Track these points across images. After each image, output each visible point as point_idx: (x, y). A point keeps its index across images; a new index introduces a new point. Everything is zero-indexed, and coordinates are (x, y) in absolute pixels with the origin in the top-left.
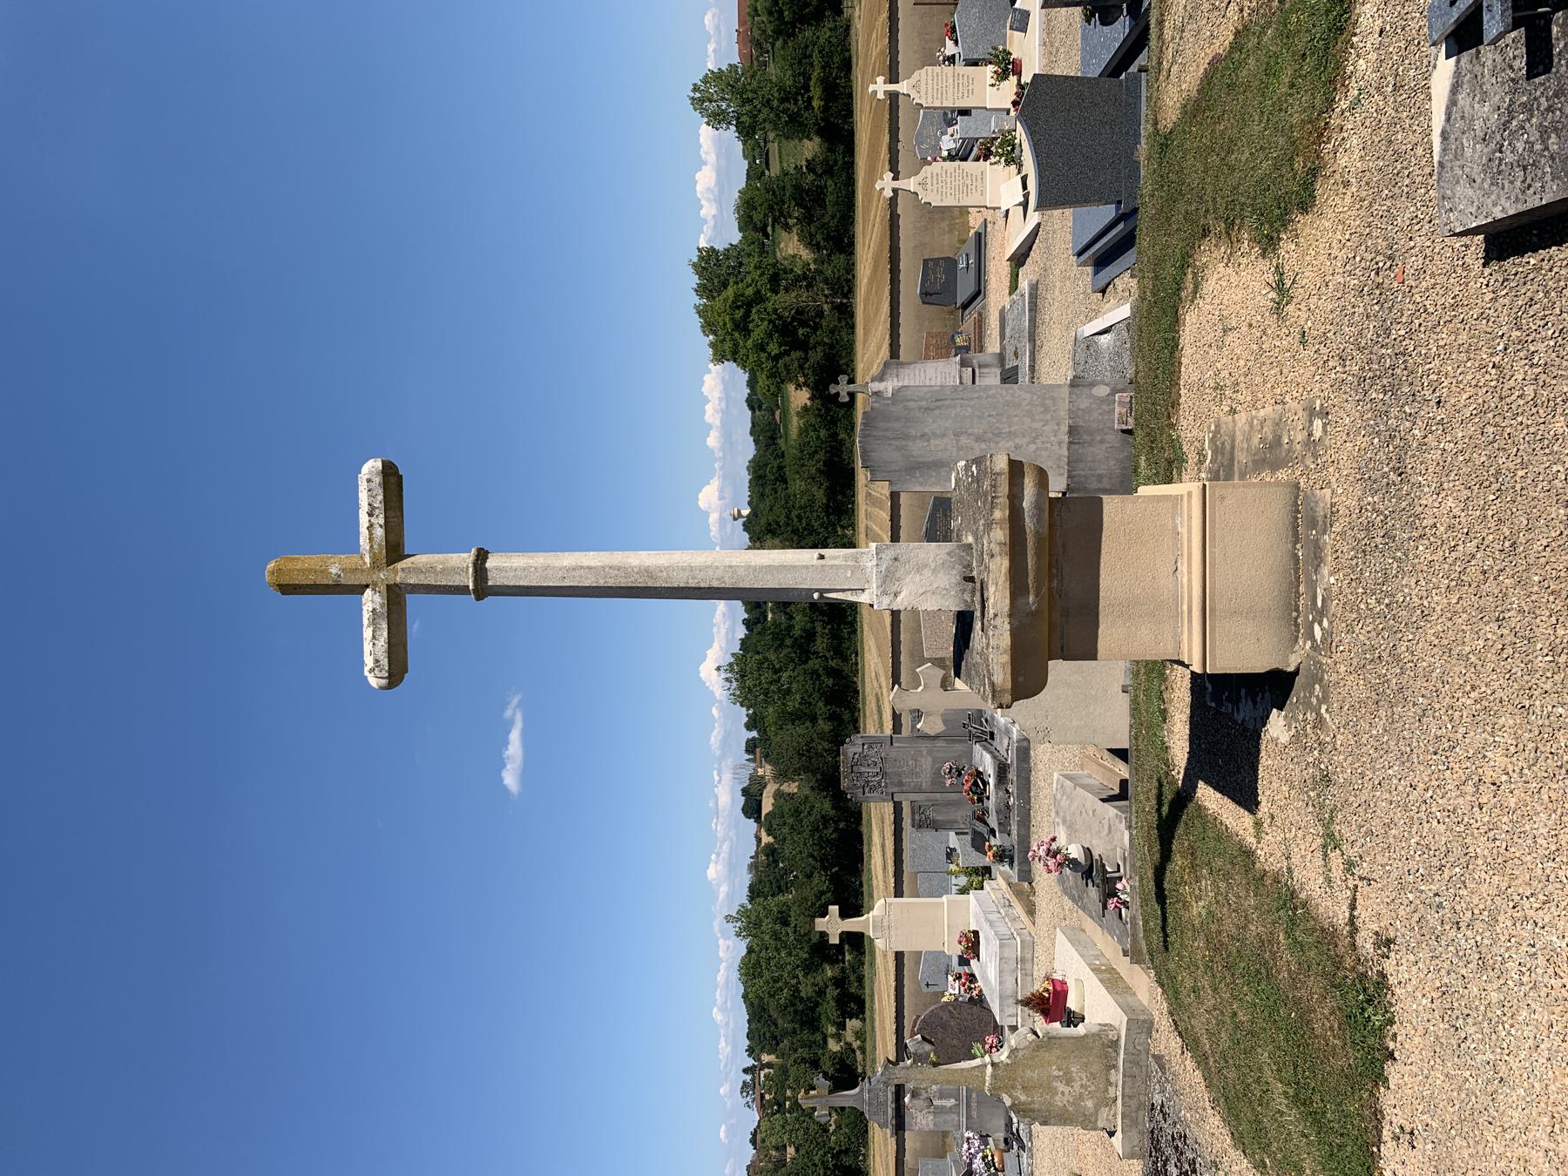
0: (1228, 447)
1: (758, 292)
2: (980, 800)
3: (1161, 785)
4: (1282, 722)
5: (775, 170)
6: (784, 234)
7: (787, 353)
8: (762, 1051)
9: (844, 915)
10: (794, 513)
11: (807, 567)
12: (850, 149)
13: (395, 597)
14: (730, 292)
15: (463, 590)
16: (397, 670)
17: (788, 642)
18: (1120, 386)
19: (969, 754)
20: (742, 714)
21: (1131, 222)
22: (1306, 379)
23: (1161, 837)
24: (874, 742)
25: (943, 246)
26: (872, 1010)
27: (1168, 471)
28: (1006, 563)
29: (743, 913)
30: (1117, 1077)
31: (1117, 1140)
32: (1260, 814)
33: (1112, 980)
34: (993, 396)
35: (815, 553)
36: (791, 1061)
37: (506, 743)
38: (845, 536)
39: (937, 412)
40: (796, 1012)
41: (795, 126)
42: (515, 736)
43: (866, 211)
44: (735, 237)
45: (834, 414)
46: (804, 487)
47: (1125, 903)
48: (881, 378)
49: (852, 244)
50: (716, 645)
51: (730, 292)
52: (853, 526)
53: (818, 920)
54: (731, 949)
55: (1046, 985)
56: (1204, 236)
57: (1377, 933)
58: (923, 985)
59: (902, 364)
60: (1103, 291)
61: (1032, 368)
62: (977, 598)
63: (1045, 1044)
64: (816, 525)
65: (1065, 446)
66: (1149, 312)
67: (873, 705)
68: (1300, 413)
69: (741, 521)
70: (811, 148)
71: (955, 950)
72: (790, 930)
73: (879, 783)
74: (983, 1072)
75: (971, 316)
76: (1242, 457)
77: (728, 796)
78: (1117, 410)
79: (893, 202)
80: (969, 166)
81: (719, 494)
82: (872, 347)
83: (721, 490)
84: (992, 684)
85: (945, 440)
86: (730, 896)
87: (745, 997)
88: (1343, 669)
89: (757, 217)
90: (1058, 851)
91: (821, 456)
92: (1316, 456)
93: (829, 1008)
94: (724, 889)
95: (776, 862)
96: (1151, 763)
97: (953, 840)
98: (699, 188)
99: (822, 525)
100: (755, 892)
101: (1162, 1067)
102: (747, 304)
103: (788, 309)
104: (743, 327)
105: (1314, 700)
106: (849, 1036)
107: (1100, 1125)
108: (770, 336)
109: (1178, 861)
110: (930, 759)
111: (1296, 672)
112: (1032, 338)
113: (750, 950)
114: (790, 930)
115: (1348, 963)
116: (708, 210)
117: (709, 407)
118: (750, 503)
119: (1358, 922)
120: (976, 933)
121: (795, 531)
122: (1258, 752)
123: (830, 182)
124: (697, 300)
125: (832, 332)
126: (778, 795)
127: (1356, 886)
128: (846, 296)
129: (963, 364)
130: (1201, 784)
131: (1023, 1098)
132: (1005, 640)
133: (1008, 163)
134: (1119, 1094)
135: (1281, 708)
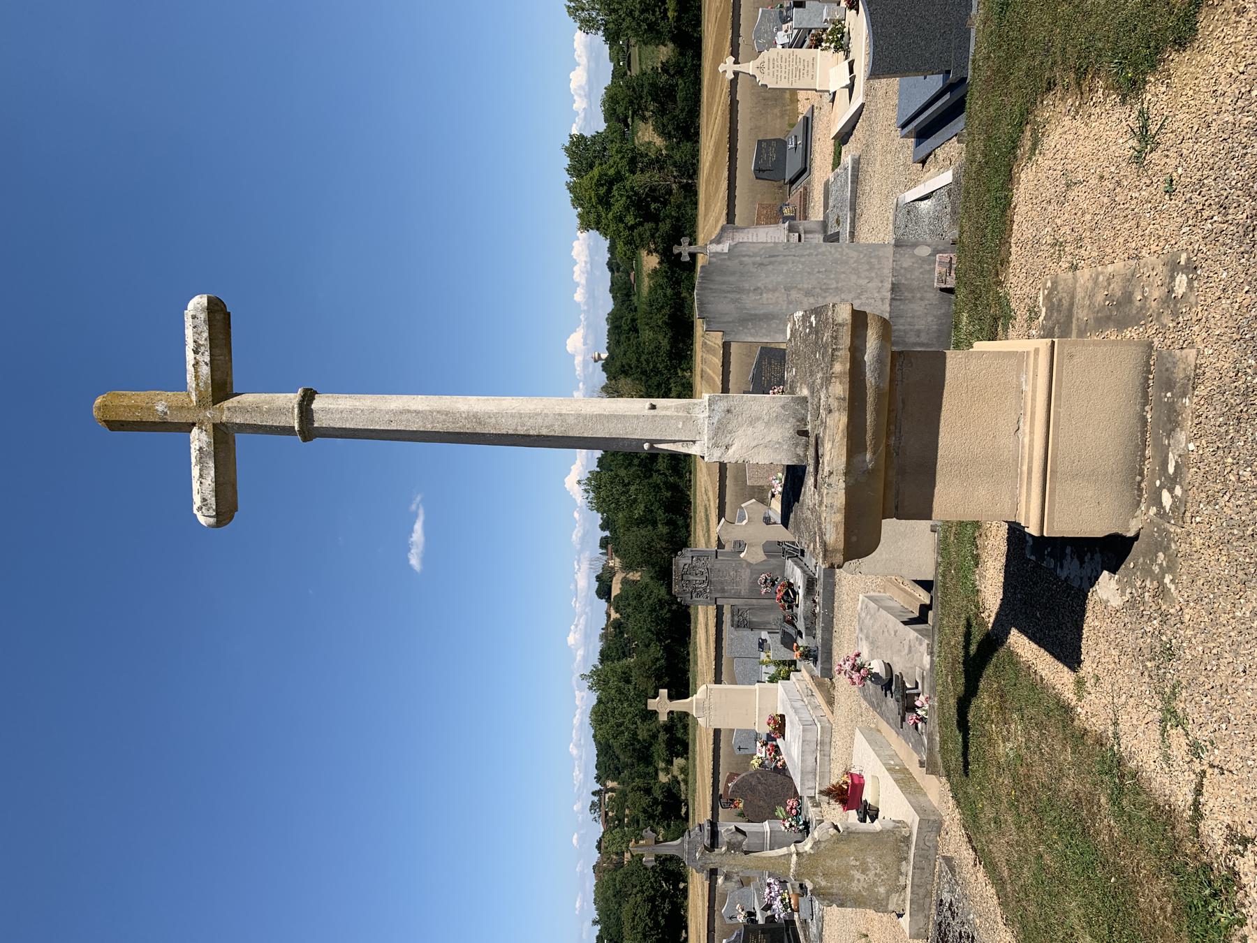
0: (1065, 303)
1: (618, 172)
2: (790, 607)
3: (969, 625)
4: (1113, 585)
5: (635, 70)
6: (642, 125)
7: (641, 224)
8: (607, 778)
9: (671, 697)
10: (643, 358)
11: (637, 417)
12: (698, 55)
13: (223, 436)
14: (596, 172)
15: (289, 430)
16: (225, 509)
17: (636, 461)
18: (940, 248)
19: (782, 567)
20: (598, 518)
21: (958, 93)
22: (1169, 231)
23: (967, 672)
24: (702, 555)
25: (774, 128)
26: (694, 751)
27: (994, 324)
28: (844, 419)
29: (595, 672)
30: (908, 868)
31: (905, 921)
32: (1082, 673)
33: (904, 780)
34: (823, 254)
35: (647, 402)
36: (629, 789)
37: (411, 531)
38: (684, 377)
39: (770, 268)
40: (634, 750)
41: (653, 34)
42: (418, 527)
43: (710, 105)
44: (602, 126)
45: (679, 272)
46: (653, 337)
47: (922, 719)
48: (718, 240)
49: (697, 134)
50: (578, 462)
51: (596, 172)
52: (691, 369)
53: (650, 701)
54: (585, 699)
55: (845, 778)
56: (1049, 89)
57: (1228, 826)
58: (736, 748)
59: (738, 229)
60: (923, 162)
61: (852, 234)
62: (811, 451)
63: (844, 836)
64: (660, 366)
65: (887, 302)
66: (978, 173)
67: (703, 514)
68: (1160, 268)
69: (601, 362)
70: (665, 52)
71: (764, 729)
72: (631, 687)
73: (705, 590)
74: (789, 861)
75: (798, 189)
76: (1081, 314)
77: (585, 582)
78: (937, 269)
79: (734, 83)
80: (804, 53)
81: (583, 341)
82: (712, 220)
83: (585, 338)
84: (824, 544)
85: (777, 294)
86: (585, 658)
87: (594, 736)
88: (1198, 541)
89: (620, 110)
90: (862, 667)
91: (666, 311)
92: (1176, 314)
93: (660, 748)
94: (580, 652)
95: (622, 633)
96: (958, 603)
97: (764, 635)
98: (573, 86)
99: (666, 367)
100: (604, 656)
101: (952, 869)
102: (610, 182)
103: (641, 188)
104: (605, 201)
105: (1156, 569)
106: (675, 770)
107: (891, 908)
108: (627, 209)
109: (984, 701)
110: (748, 571)
111: (1136, 537)
112: (853, 209)
113: (600, 701)
114: (631, 687)
115: (1189, 848)
116: (579, 104)
117: (576, 269)
118: (608, 349)
119: (1205, 810)
120: (782, 717)
121: (644, 373)
122: (1084, 611)
123: (680, 81)
124: (568, 178)
125: (679, 207)
126: (625, 582)
127: (1204, 772)
128: (691, 177)
129: (791, 229)
130: (1014, 631)
131: (823, 883)
132: (840, 499)
133: (836, 50)
134: (909, 883)
135: (1113, 570)
